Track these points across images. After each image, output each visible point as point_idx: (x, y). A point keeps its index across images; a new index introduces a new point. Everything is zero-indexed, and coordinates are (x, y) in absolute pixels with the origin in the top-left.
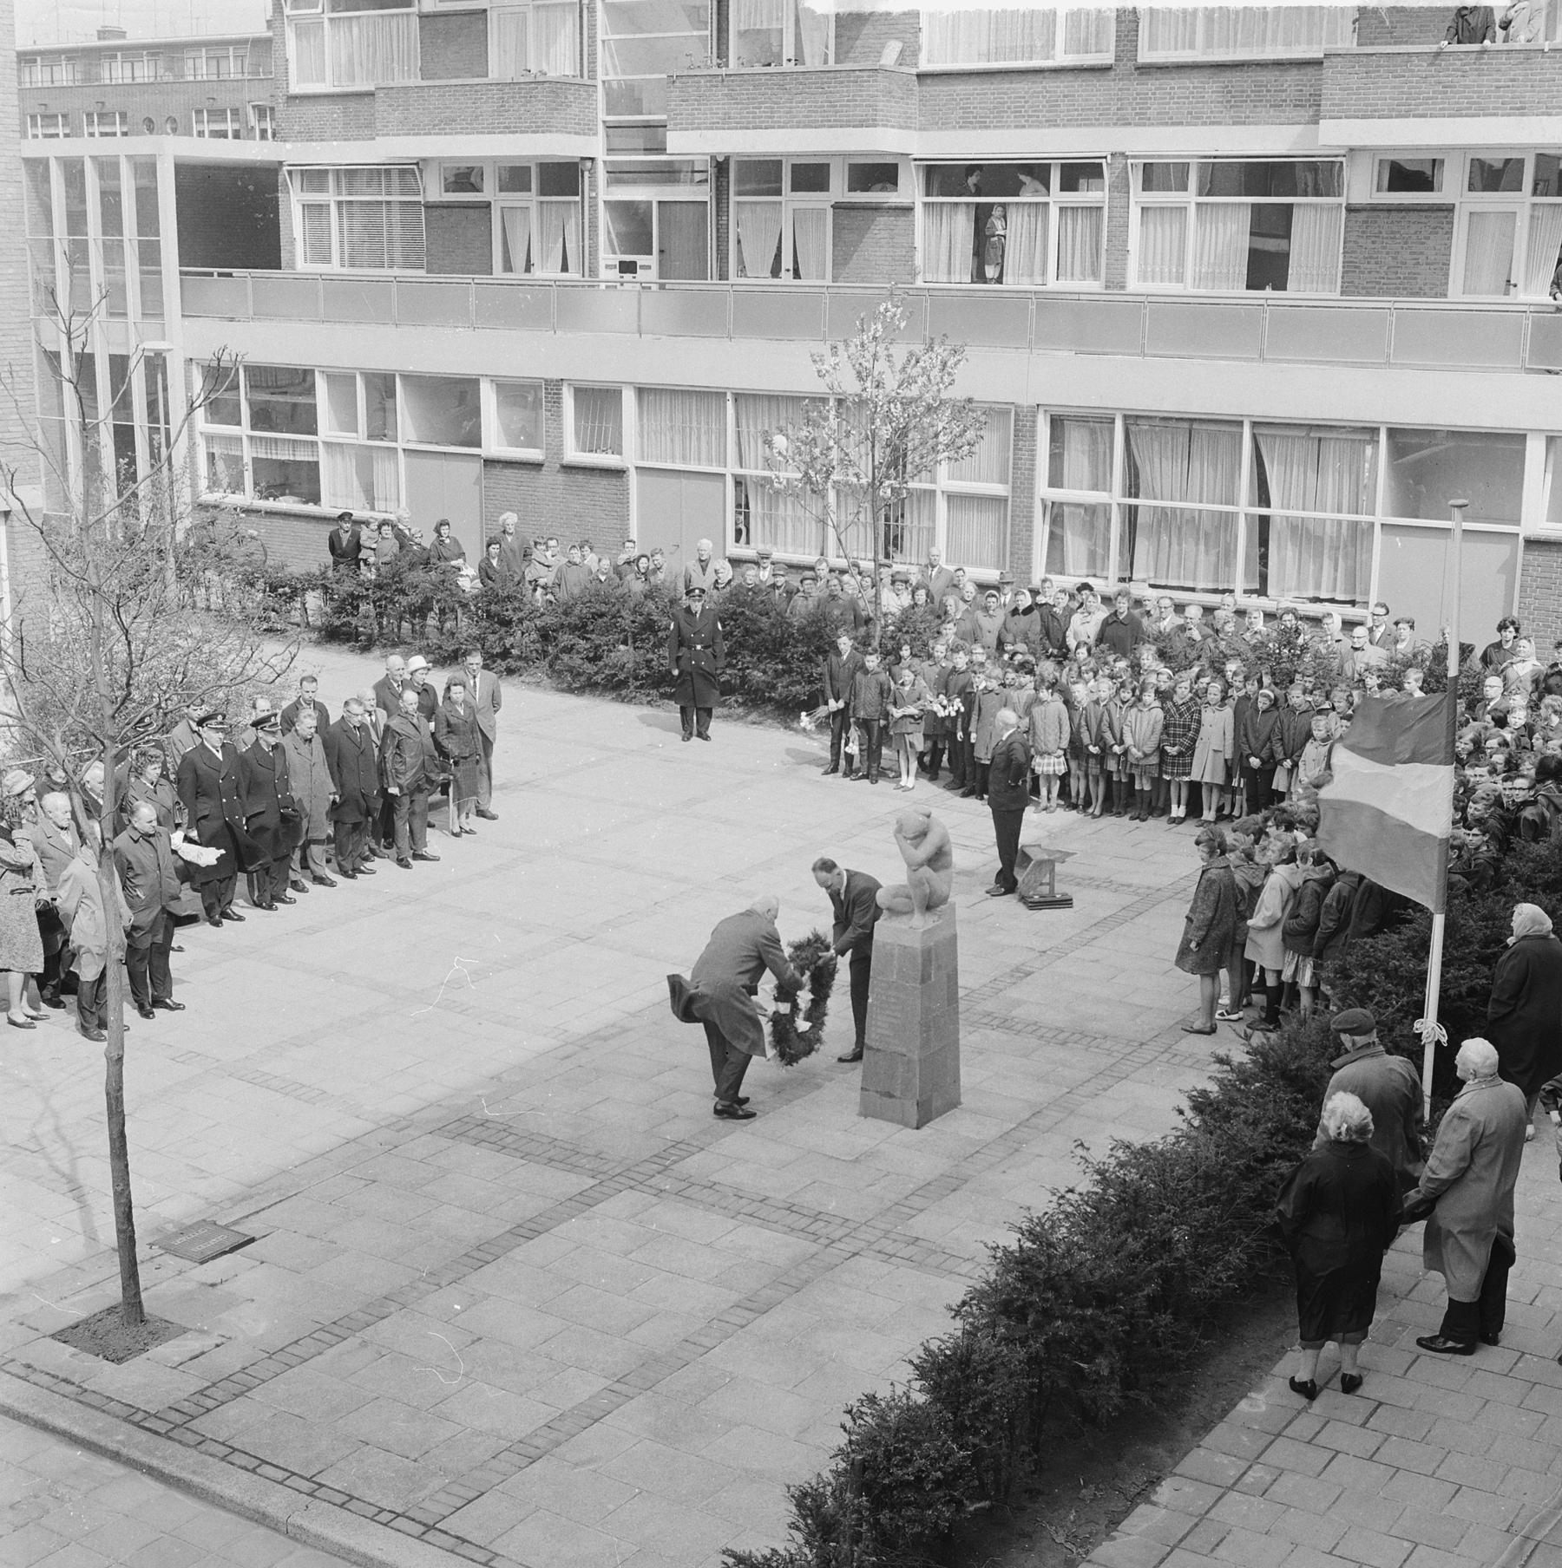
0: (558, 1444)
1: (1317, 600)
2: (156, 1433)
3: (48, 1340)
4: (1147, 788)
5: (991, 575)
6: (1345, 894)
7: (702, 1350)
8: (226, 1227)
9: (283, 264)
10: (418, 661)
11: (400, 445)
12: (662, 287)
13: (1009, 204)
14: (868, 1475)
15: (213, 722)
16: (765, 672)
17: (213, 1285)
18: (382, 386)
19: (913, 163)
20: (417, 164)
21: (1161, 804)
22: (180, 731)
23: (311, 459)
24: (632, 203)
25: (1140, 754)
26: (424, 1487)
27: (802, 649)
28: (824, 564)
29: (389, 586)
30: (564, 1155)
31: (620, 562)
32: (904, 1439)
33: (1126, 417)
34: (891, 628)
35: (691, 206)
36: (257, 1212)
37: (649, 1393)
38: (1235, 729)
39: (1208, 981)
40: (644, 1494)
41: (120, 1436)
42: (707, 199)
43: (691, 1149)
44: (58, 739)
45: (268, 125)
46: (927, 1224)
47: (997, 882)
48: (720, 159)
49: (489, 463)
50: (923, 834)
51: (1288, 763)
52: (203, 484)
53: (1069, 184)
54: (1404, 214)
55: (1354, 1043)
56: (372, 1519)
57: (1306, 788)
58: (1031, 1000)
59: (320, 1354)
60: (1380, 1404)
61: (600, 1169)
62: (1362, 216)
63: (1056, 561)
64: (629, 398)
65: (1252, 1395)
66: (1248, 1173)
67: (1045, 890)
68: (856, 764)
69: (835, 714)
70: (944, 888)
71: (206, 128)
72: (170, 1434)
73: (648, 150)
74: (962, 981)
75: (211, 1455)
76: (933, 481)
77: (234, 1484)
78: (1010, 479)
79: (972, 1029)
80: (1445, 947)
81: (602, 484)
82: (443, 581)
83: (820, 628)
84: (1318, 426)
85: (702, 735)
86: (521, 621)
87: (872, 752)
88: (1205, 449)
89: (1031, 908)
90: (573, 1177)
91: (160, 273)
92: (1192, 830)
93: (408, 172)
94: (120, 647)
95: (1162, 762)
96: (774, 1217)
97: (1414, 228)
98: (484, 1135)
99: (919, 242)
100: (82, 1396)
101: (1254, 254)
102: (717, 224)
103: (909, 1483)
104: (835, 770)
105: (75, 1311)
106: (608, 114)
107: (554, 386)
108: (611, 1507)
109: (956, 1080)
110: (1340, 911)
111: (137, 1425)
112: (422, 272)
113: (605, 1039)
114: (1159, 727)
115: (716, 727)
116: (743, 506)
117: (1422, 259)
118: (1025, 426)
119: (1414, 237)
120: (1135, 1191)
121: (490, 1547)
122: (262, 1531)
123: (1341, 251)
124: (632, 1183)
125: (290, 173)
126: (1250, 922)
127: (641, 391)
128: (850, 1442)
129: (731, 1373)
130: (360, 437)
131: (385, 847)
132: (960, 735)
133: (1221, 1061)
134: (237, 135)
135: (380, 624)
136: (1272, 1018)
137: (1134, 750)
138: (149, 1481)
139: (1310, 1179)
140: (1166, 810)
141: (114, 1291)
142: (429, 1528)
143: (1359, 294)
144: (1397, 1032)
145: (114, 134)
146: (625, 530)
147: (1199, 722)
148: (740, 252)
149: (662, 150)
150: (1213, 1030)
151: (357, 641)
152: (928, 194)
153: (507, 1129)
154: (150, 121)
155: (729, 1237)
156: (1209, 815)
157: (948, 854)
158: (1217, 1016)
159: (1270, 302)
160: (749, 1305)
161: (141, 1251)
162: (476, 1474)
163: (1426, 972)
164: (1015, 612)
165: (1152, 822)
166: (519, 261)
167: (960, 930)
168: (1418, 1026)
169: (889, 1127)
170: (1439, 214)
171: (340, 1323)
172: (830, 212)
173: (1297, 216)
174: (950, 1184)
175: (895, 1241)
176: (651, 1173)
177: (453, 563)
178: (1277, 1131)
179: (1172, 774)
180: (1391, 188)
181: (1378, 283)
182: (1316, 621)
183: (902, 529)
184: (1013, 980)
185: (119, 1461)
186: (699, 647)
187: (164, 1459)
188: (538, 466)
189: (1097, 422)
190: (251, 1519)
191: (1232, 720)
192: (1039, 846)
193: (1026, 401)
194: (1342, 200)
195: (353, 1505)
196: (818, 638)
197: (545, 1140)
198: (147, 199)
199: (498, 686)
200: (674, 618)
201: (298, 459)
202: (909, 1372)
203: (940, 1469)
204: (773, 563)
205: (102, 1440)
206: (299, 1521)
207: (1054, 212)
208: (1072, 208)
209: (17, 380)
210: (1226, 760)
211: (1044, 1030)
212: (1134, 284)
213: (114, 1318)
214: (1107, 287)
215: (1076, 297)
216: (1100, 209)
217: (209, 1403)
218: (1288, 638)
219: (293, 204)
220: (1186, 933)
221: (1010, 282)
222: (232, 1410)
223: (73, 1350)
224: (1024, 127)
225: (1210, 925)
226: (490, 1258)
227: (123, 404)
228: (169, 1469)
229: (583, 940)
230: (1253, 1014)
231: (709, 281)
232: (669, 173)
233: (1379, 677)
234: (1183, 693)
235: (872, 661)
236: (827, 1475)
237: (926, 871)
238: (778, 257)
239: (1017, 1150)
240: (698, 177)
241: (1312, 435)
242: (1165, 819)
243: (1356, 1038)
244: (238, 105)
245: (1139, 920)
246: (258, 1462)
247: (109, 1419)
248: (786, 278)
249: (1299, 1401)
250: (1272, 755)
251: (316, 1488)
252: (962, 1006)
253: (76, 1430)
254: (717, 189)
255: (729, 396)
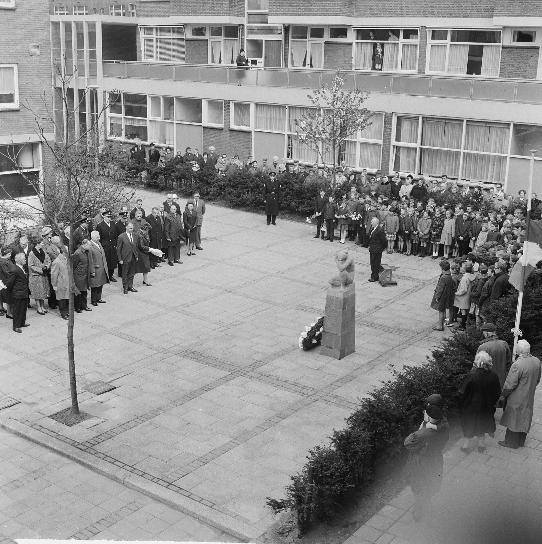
0: (213, 459)
1: (486, 183)
2: (82, 449)
3: (48, 418)
4: (425, 246)
5: (374, 171)
6: (490, 284)
7: (263, 430)
8: (107, 383)
9: (137, 59)
10: (175, 196)
11: (175, 122)
12: (265, 69)
13: (385, 43)
14: (315, 473)
15: (107, 214)
16: (296, 202)
17: (102, 402)
18: (169, 101)
19: (352, 28)
20: (183, 26)
21: (429, 252)
22: (97, 217)
23: (145, 126)
24: (256, 40)
25: (423, 234)
26: (169, 471)
27: (308, 195)
28: (316, 166)
29: (169, 170)
30: (218, 364)
31: (248, 164)
32: (328, 462)
33: (423, 118)
34: (339, 188)
35: (276, 42)
36: (117, 379)
37: (245, 443)
38: (456, 227)
39: (442, 313)
40: (242, 476)
41: (70, 450)
42: (281, 39)
43: (263, 363)
44: (55, 218)
45: (134, 11)
46: (341, 392)
47: (371, 277)
48: (286, 26)
49: (205, 128)
50: (345, 259)
51: (474, 238)
52: (108, 134)
53: (406, 37)
54: (522, 49)
55: (488, 334)
56: (151, 480)
57: (478, 248)
58: (381, 317)
59: (136, 426)
60: (491, 457)
61: (232, 369)
62: (508, 50)
63: (397, 167)
64: (252, 107)
65: (448, 452)
66: (450, 379)
67: (388, 280)
68: (325, 235)
69: (318, 217)
70: (352, 278)
71: (114, 11)
72: (86, 450)
73: (262, 22)
74: (357, 309)
75: (99, 458)
76: (356, 138)
77: (107, 468)
78: (382, 138)
79: (360, 326)
80: (523, 304)
81: (242, 137)
82: (188, 168)
83: (315, 188)
84: (489, 122)
85: (274, 223)
86: (214, 183)
87: (330, 230)
88: (450, 129)
89: (383, 286)
90: (223, 371)
91: (96, 61)
92: (440, 260)
93: (179, 29)
94: (77, 188)
95: (430, 237)
96: (289, 387)
97: (525, 54)
98: (194, 356)
99: (353, 56)
100: (58, 437)
101: (470, 62)
102: (285, 48)
103: (328, 476)
104: (318, 236)
105: (57, 408)
106: (249, 10)
107: (228, 103)
108: (230, 480)
109: (354, 343)
110: (489, 290)
111: (76, 447)
112: (184, 63)
113: (236, 325)
114: (430, 225)
115: (277, 220)
116: (290, 147)
117: (528, 65)
118: (388, 120)
119: (525, 57)
120: (411, 384)
121: (190, 491)
122: (115, 483)
123: (500, 61)
124: (242, 374)
125: (140, 28)
126: (456, 293)
127: (257, 105)
128: (310, 462)
129: (273, 438)
130: (161, 119)
131: (165, 258)
132: (361, 226)
133: (445, 340)
134: (124, 15)
135: (166, 182)
136: (463, 325)
137: (421, 233)
138: (78, 465)
139: (470, 380)
140: (432, 253)
141: (69, 403)
142: (170, 484)
143: (506, 77)
144: (505, 332)
145: (83, 14)
146: (250, 152)
147: (443, 223)
148: (292, 58)
149: (267, 22)
150: (443, 330)
151: (158, 188)
152: (357, 40)
153: (201, 354)
154: (95, 9)
155: (274, 393)
156: (446, 256)
157: (353, 266)
158: (444, 325)
159: (474, 79)
160: (280, 416)
161: (79, 390)
162: (186, 467)
163: (516, 313)
164: (382, 183)
165: (426, 258)
166: (217, 59)
167: (356, 292)
168: (512, 330)
169: (331, 359)
170: (534, 50)
171: (143, 416)
172: (324, 45)
173: (485, 51)
174: (350, 378)
175: (330, 396)
176: (249, 371)
177: (191, 162)
178: (461, 364)
179: (434, 241)
180: (518, 40)
181: (513, 73)
182: (487, 190)
183: (345, 154)
184: (375, 310)
185: (69, 458)
186: (273, 193)
187: (84, 458)
188: (221, 129)
189: (413, 119)
190: (112, 479)
191: (454, 224)
192: (387, 265)
193: (388, 111)
194: (501, 44)
195: (145, 476)
196: (314, 190)
197: (214, 359)
198: (92, 35)
199: (205, 206)
200: (265, 183)
201: (140, 126)
202: (329, 441)
203: (339, 472)
204: (300, 165)
205: (64, 451)
206: (128, 480)
207: (401, 46)
208: (407, 45)
209: (46, 97)
210: (452, 237)
211: (385, 328)
212: (428, 72)
213: (69, 413)
214: (418, 72)
215: (407, 76)
216: (417, 45)
217: (99, 441)
218: (477, 196)
219: (142, 36)
220: (434, 296)
221: (385, 70)
222: (107, 443)
223: (55, 421)
224: (391, 17)
225: (442, 293)
226: (193, 397)
227: (82, 105)
228: (85, 461)
229: (229, 292)
230: (457, 325)
231: (281, 68)
232: (270, 30)
233: (505, 210)
234: (437, 214)
235: (331, 199)
236: (301, 473)
237: (346, 272)
238: (305, 60)
239: (373, 368)
240: (279, 32)
241: (487, 125)
242: (431, 256)
243: (489, 333)
244: (125, 4)
245: (420, 291)
246: (114, 460)
247: (67, 444)
248: (308, 67)
249: (463, 454)
250: (468, 236)
251: (133, 470)
252: (356, 319)
253: (55, 448)
254: (285, 36)
255: (287, 107)
